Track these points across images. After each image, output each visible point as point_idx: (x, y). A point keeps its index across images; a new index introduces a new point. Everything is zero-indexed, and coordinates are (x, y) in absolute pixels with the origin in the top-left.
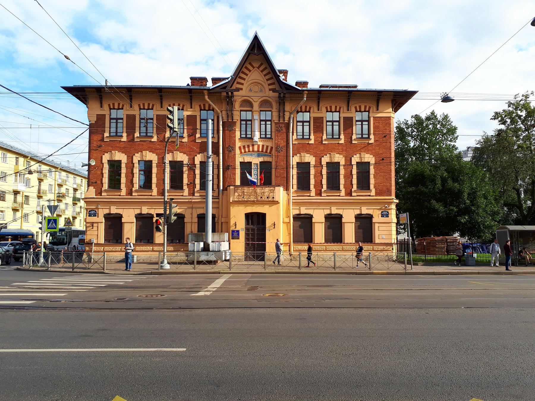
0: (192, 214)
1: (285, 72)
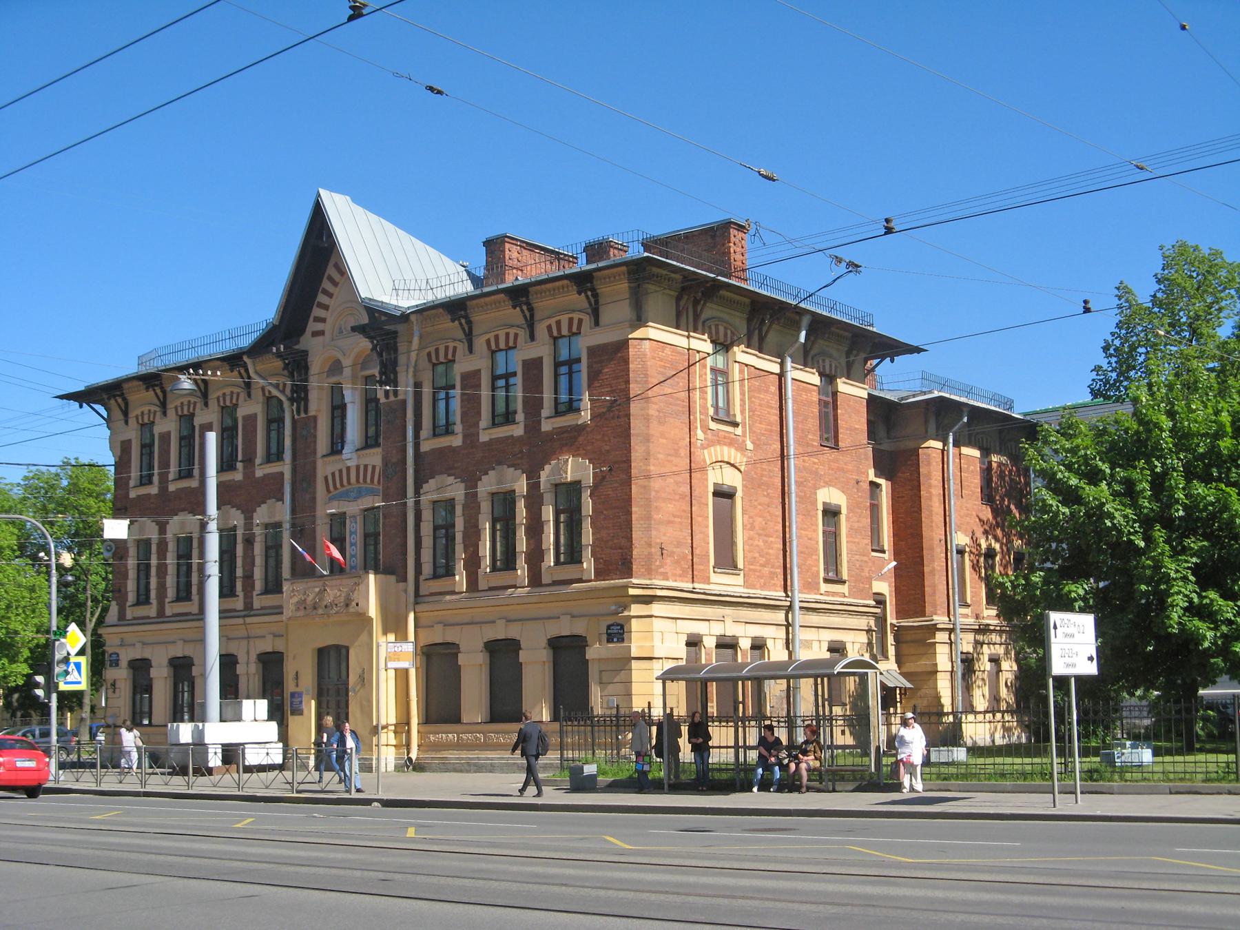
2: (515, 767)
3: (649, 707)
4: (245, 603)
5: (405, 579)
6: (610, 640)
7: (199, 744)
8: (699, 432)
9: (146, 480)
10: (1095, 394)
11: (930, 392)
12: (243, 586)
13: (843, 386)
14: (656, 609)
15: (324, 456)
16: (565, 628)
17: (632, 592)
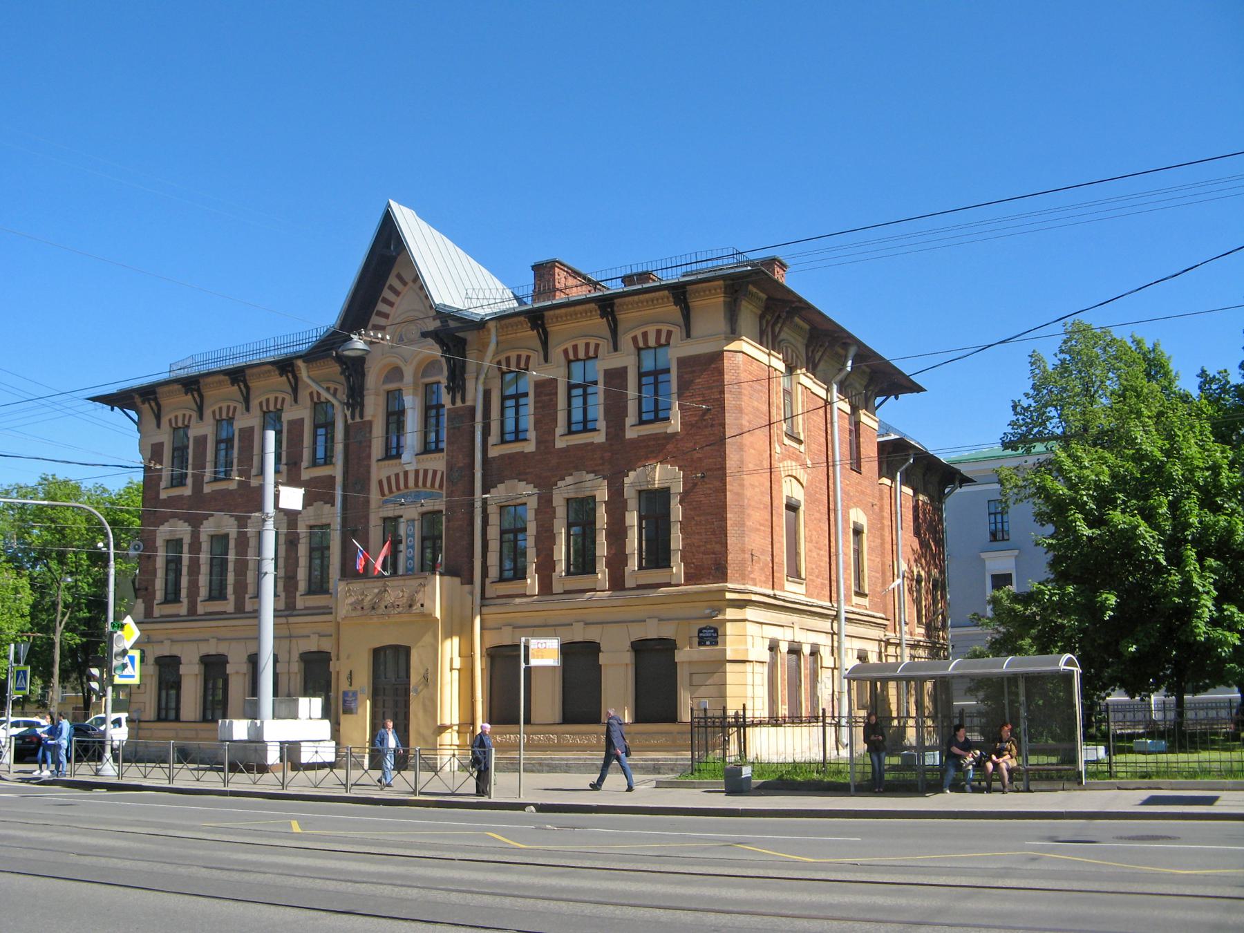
2: (594, 768)
3: (744, 709)
4: (286, 602)
5: (471, 582)
6: (702, 643)
7: (257, 742)
8: (777, 446)
9: (178, 481)
10: (1006, 445)
11: (888, 434)
12: (284, 586)
13: (865, 418)
14: (750, 613)
15: (379, 460)
16: (652, 631)
17: (729, 596)
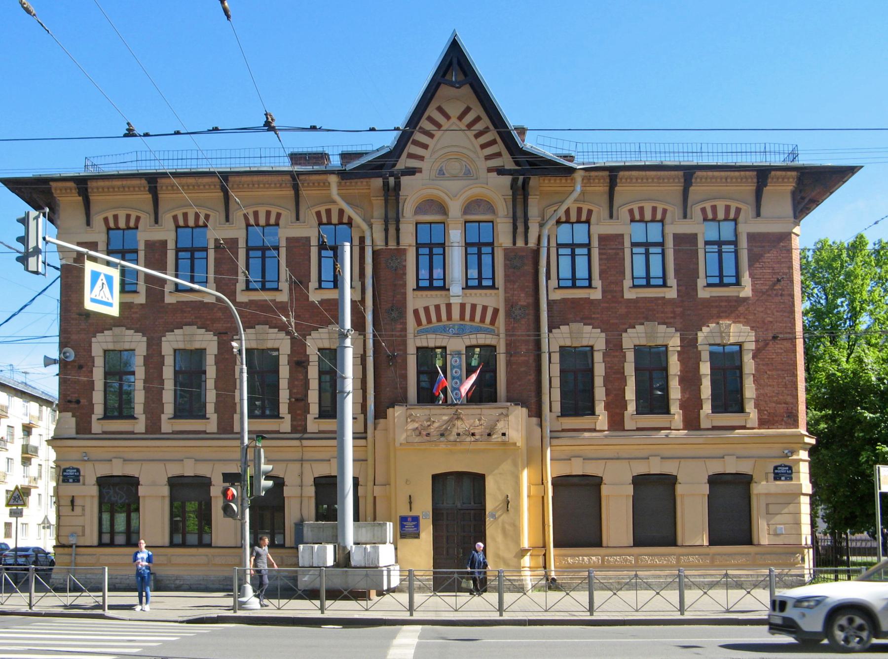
0: (301, 475)
1: (522, 131)
6: (777, 477)
